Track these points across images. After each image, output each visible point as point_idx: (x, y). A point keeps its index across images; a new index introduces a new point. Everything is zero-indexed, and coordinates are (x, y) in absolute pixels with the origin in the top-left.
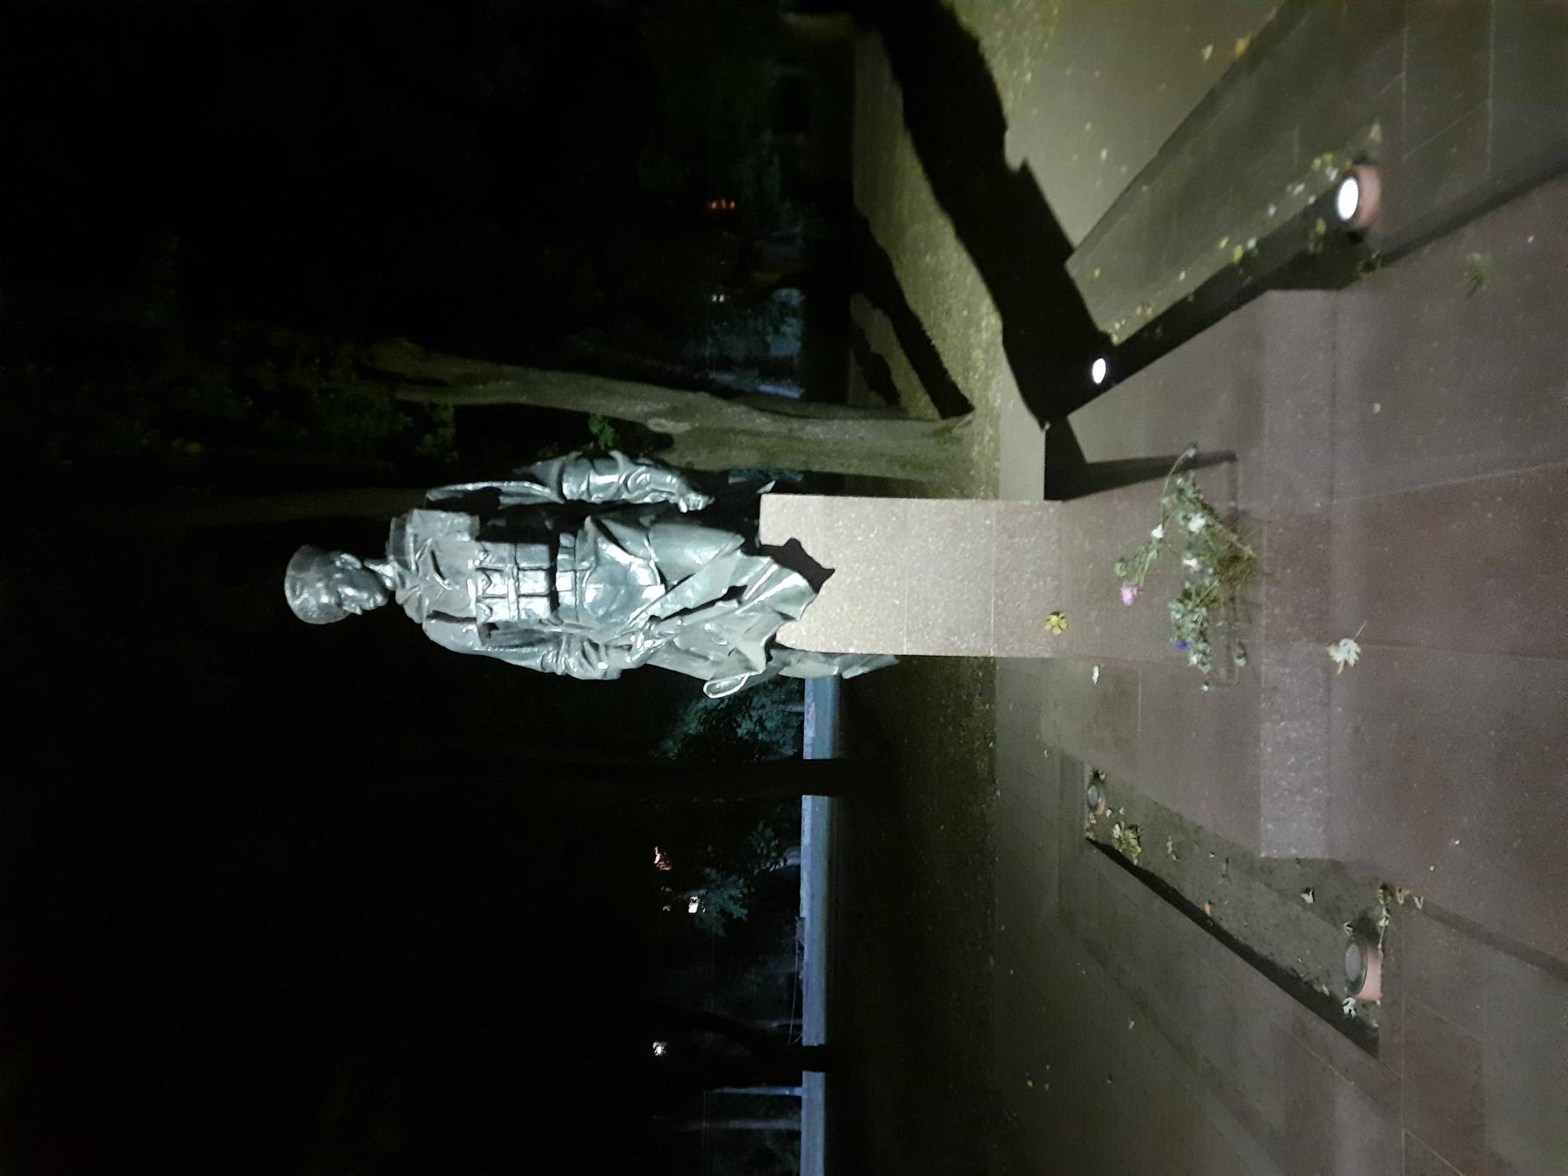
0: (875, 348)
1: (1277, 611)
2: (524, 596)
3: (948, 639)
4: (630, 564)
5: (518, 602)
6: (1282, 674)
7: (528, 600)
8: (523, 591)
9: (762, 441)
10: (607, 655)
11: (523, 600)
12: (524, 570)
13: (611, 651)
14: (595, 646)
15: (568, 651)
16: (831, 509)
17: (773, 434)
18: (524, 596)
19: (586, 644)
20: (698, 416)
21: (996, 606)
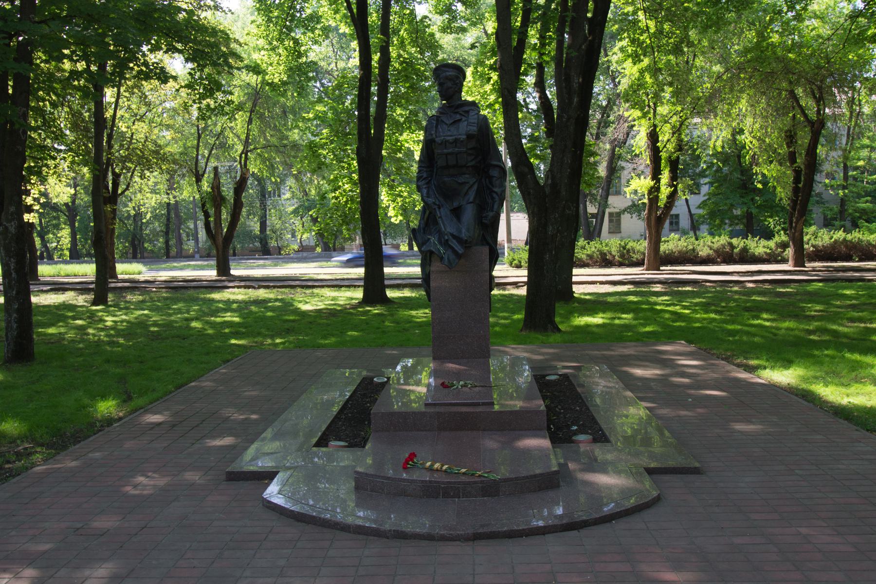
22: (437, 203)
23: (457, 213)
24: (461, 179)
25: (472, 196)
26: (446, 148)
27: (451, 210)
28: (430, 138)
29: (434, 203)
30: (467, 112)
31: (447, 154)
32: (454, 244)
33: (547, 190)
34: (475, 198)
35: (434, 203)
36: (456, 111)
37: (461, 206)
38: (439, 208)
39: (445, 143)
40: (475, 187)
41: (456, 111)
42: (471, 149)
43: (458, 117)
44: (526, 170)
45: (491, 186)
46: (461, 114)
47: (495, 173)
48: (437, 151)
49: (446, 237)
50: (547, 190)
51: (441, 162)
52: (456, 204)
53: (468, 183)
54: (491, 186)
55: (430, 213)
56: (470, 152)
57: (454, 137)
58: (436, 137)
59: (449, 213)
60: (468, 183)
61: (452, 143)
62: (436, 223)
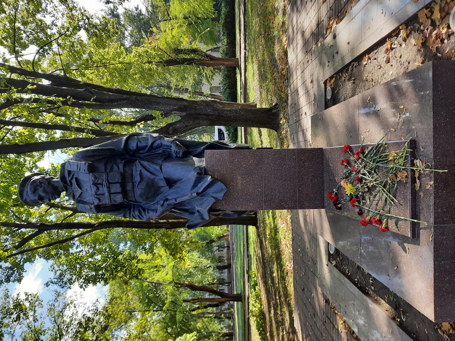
0: (346, 337)
1: (439, 211)
2: (112, 193)
3: (281, 204)
4: (155, 179)
5: (110, 197)
6: (443, 239)
7: (114, 195)
8: (112, 191)
9: (210, 117)
10: (148, 213)
11: (112, 195)
12: (111, 183)
13: (150, 211)
14: (144, 210)
15: (134, 211)
16: (232, 154)
17: (213, 115)
18: (112, 193)
19: (140, 208)
20: (189, 110)
21: (299, 190)
22: (162, 202)
23: (170, 183)
24: (137, 179)
25: (154, 167)
26: (104, 194)
27: (170, 188)
28: (94, 209)
29: (162, 205)
30: (69, 172)
31: (110, 194)
32: (201, 187)
33: (184, 114)
34: (157, 164)
35: (162, 205)
36: (69, 183)
37: (165, 178)
38: (167, 200)
39: (98, 196)
40: (145, 163)
41: (69, 183)
42: (106, 169)
43: (74, 181)
44: (171, 128)
45: (147, 149)
46: (72, 179)
47: (133, 145)
48: (106, 201)
49: (195, 195)
50: (184, 114)
51: (119, 199)
52: (163, 183)
53: (141, 171)
54: (147, 149)
55: (174, 208)
56: (109, 168)
57: (152, 177)
58: (93, 203)
59: (172, 190)
60: (141, 171)
61: (98, 189)
62: (181, 204)
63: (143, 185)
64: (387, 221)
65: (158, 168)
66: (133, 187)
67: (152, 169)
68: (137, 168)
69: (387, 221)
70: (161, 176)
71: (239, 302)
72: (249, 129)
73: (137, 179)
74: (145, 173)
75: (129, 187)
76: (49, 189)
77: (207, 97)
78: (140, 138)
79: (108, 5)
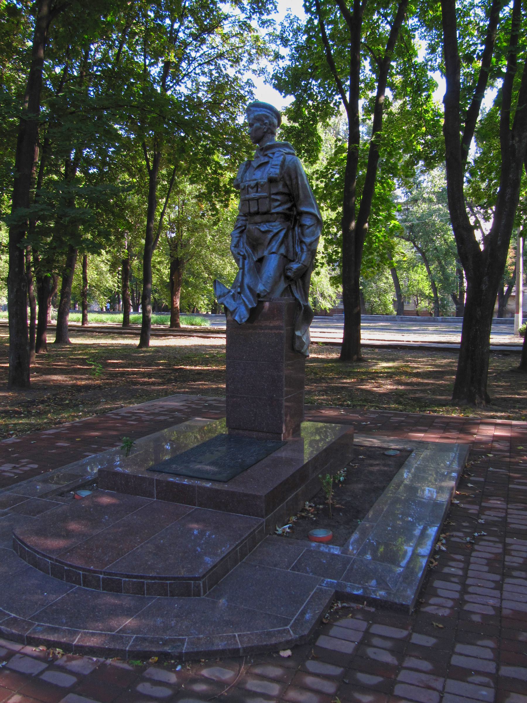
34: (278, 249)
36: (266, 153)
52: (259, 255)
63: (256, 234)
64: (274, 194)
65: (274, 250)
66: (256, 223)
67: (273, 243)
68: (276, 226)
69: (274, 194)
70: (266, 253)
71: (6, 313)
72: (8, 330)
73: (264, 228)
74: (270, 236)
75: (258, 218)
76: (260, 133)
77: (50, 423)
78: (78, 641)
79: (329, 284)
